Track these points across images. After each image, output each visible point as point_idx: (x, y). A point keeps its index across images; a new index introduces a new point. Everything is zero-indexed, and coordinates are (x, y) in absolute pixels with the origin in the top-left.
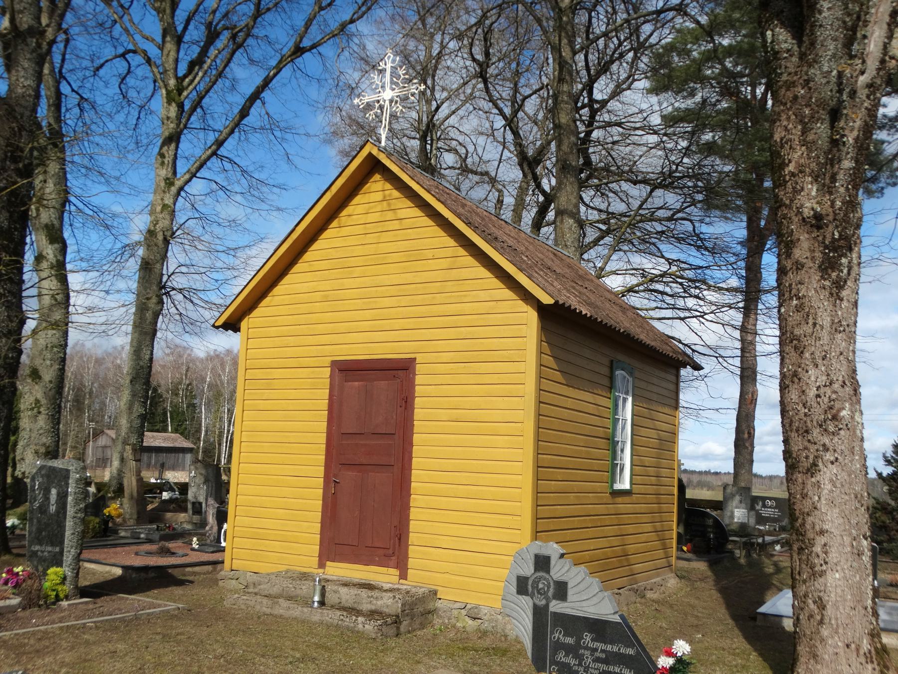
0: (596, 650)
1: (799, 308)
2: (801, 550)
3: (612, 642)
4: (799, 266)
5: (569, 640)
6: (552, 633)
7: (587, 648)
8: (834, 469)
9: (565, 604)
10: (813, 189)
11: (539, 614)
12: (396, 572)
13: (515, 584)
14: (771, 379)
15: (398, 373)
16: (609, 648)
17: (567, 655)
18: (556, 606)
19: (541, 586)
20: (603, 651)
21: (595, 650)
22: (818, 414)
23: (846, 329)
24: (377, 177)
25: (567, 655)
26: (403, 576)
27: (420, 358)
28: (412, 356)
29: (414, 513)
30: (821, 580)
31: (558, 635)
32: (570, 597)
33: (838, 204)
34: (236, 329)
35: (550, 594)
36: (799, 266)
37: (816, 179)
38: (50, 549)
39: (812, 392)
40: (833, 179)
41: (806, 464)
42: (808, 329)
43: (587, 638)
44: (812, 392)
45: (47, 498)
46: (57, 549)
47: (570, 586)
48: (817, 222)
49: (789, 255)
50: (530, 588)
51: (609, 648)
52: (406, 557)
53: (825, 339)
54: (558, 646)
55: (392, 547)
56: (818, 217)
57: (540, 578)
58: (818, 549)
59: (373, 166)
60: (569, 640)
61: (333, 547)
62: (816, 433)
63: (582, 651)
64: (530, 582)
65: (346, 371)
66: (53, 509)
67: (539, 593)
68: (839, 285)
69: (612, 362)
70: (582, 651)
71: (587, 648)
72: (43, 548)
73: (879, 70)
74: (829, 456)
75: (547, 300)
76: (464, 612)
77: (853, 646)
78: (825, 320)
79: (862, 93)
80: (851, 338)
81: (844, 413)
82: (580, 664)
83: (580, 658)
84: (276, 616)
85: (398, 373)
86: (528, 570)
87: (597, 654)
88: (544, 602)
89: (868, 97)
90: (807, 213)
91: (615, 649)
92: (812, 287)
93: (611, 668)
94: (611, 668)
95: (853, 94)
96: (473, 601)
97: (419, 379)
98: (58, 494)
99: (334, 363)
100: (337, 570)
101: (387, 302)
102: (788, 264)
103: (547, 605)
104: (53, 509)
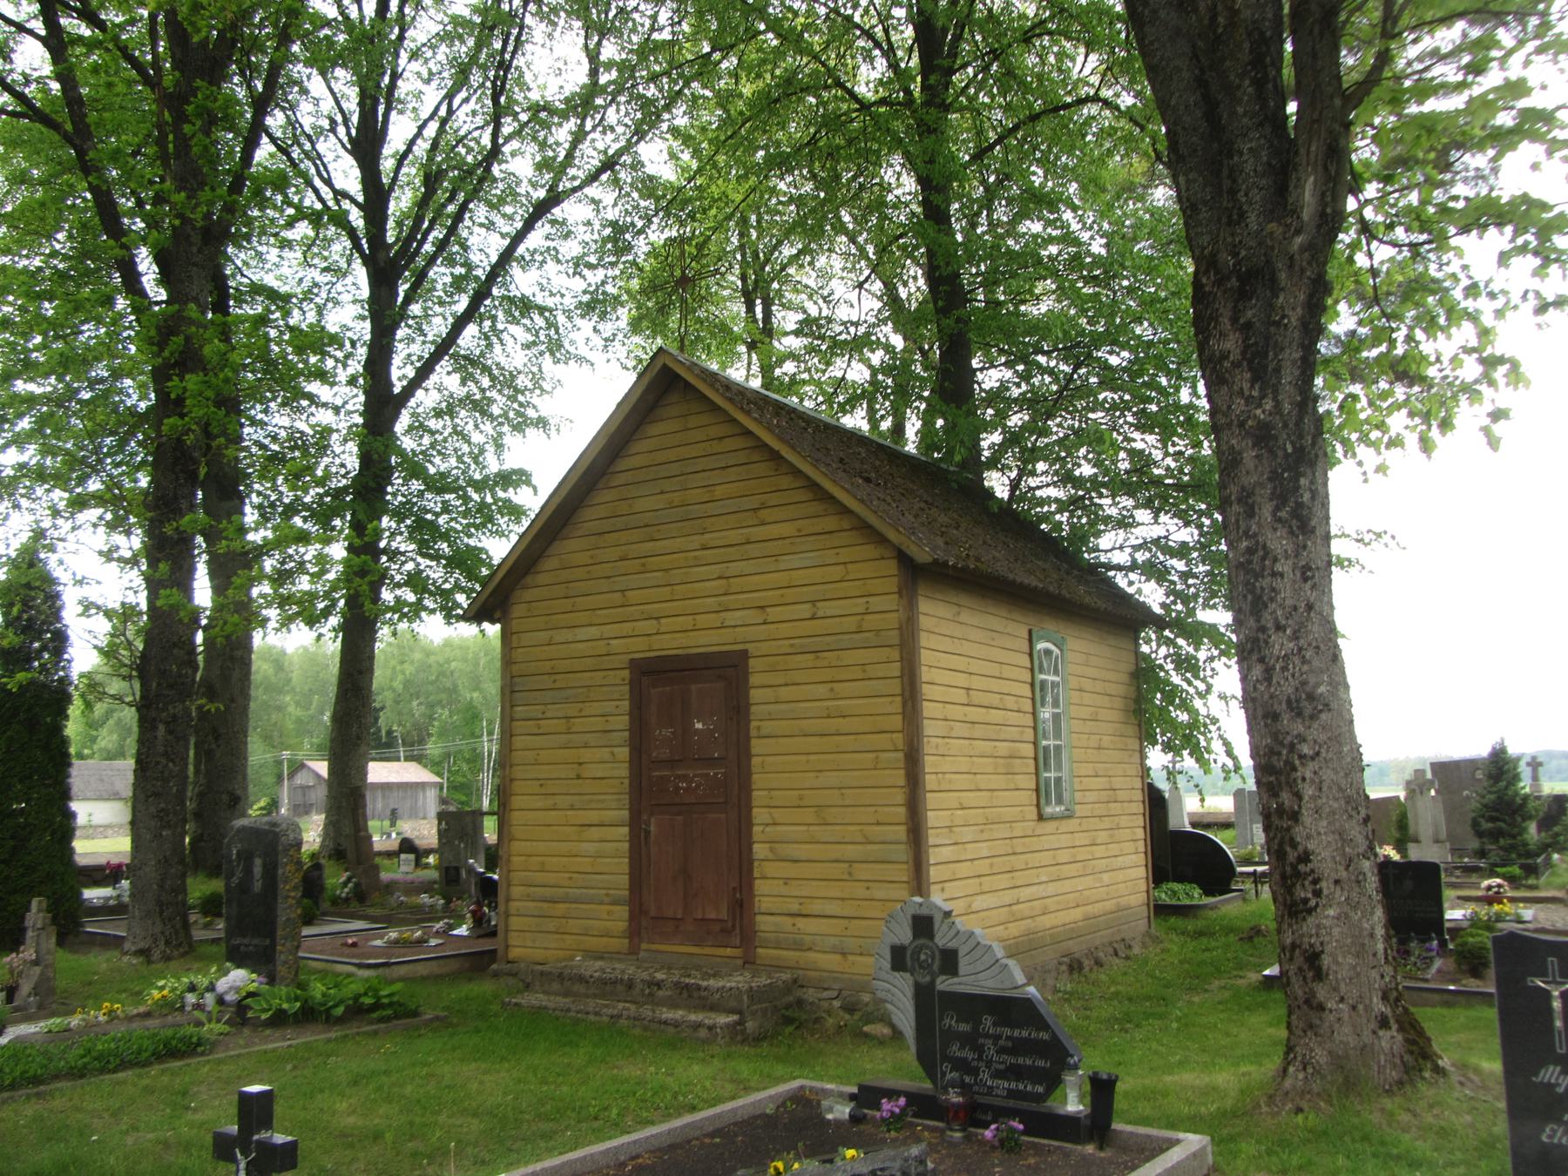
0: (1000, 1037)
3: (1021, 1027)
5: (964, 1027)
6: (941, 1019)
7: (987, 1036)
9: (956, 980)
11: (924, 997)
13: (888, 957)
15: (729, 671)
16: (1016, 1033)
17: (962, 1047)
18: (944, 984)
19: (923, 957)
20: (1008, 1038)
21: (997, 1038)
25: (962, 1047)
28: (741, 647)
30: (1311, 920)
31: (950, 1022)
32: (962, 969)
33: (1287, 407)
35: (936, 966)
38: (256, 941)
43: (987, 1022)
45: (248, 871)
46: (268, 942)
47: (961, 954)
50: (909, 964)
51: (1016, 1033)
54: (950, 1036)
57: (921, 948)
60: (964, 1027)
63: (981, 1041)
64: (909, 953)
66: (258, 886)
67: (921, 967)
69: (1030, 632)
70: (981, 1041)
71: (987, 1036)
72: (246, 941)
73: (1319, 227)
76: (836, 1004)
77: (1361, 1007)
81: (1322, 689)
82: (980, 1058)
83: (979, 1050)
84: (660, 1022)
85: (729, 671)
86: (904, 935)
87: (1002, 1042)
88: (928, 979)
89: (1309, 263)
91: (1025, 1034)
93: (1020, 1061)
94: (1020, 1061)
97: (754, 680)
98: (265, 866)
103: (933, 983)
104: (258, 886)
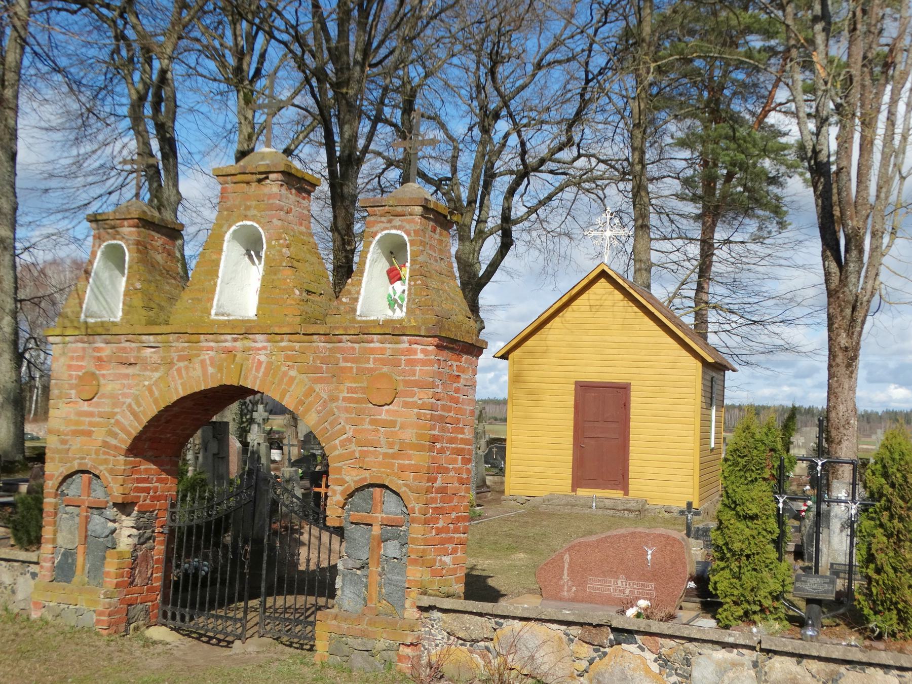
1: (837, 381)
2: (833, 473)
4: (838, 365)
8: (847, 442)
10: (844, 335)
12: (622, 492)
14: (30, 186)
22: (842, 422)
23: (852, 389)
24: (603, 280)
26: (626, 493)
27: (633, 383)
29: (631, 462)
34: (507, 359)
36: (838, 365)
37: (845, 330)
39: (841, 414)
40: (853, 333)
41: (837, 441)
42: (840, 389)
44: (841, 414)
48: (846, 349)
49: (834, 360)
52: (627, 485)
53: (846, 392)
55: (619, 477)
56: (846, 348)
58: (840, 472)
59: (603, 274)
61: (578, 482)
62: (841, 429)
65: (584, 389)
68: (852, 373)
74: (845, 438)
75: (710, 360)
78: (846, 386)
79: (865, 304)
80: (854, 393)
90: (843, 346)
92: (842, 370)
95: (861, 304)
96: (667, 504)
97: (632, 394)
99: (576, 383)
100: (582, 492)
101: (612, 351)
102: (834, 364)
